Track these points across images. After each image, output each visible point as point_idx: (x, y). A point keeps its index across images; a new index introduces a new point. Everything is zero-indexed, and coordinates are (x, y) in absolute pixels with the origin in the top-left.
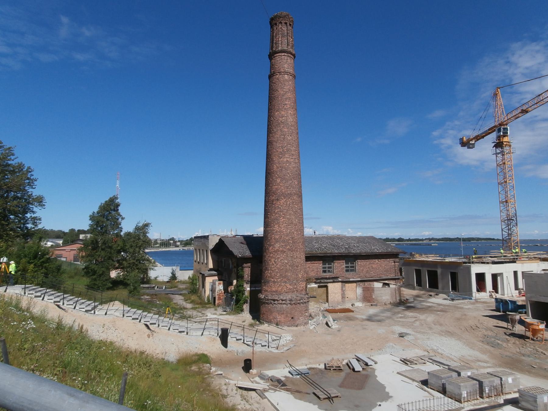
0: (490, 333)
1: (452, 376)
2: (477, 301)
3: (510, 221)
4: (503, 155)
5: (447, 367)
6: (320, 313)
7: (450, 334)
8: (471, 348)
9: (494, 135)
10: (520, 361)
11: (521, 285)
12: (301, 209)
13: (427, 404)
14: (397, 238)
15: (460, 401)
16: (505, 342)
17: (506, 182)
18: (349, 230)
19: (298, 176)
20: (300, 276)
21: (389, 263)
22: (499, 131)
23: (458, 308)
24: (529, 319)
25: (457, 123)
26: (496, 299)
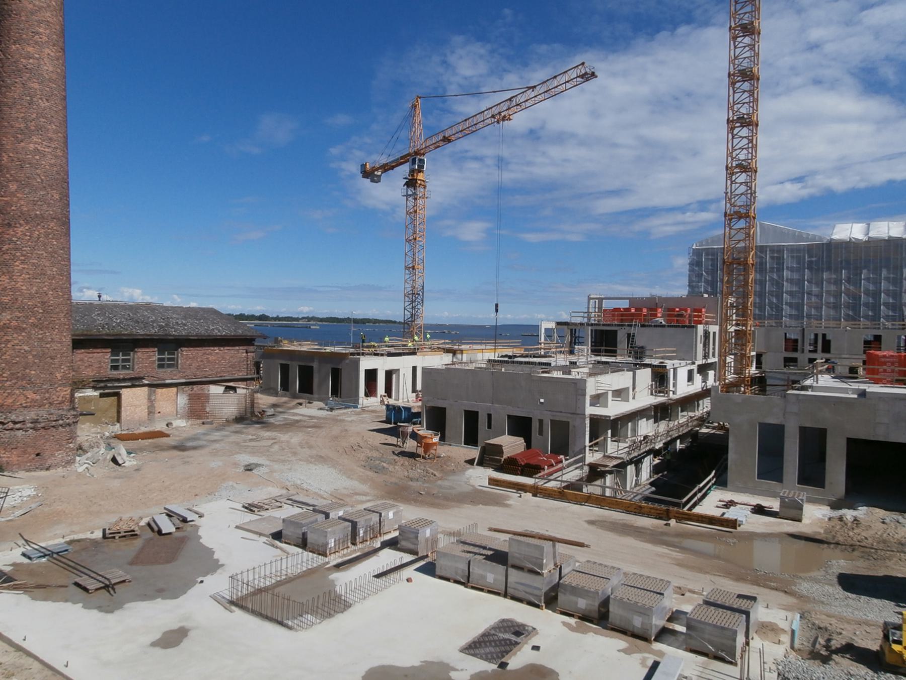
0: (375, 454)
1: (317, 520)
2: (363, 410)
3: (415, 297)
4: (415, 199)
5: (311, 508)
6: (101, 442)
7: (321, 459)
8: (348, 477)
9: (405, 169)
10: (405, 488)
11: (419, 387)
12: (67, 249)
13: (276, 567)
14: (257, 314)
15: (324, 554)
16: (391, 464)
17: (415, 239)
18: (175, 296)
19: (63, 184)
20: (59, 376)
21: (238, 354)
22: (414, 162)
23: (337, 421)
24: (423, 431)
25: (368, 140)
26: (388, 406)
